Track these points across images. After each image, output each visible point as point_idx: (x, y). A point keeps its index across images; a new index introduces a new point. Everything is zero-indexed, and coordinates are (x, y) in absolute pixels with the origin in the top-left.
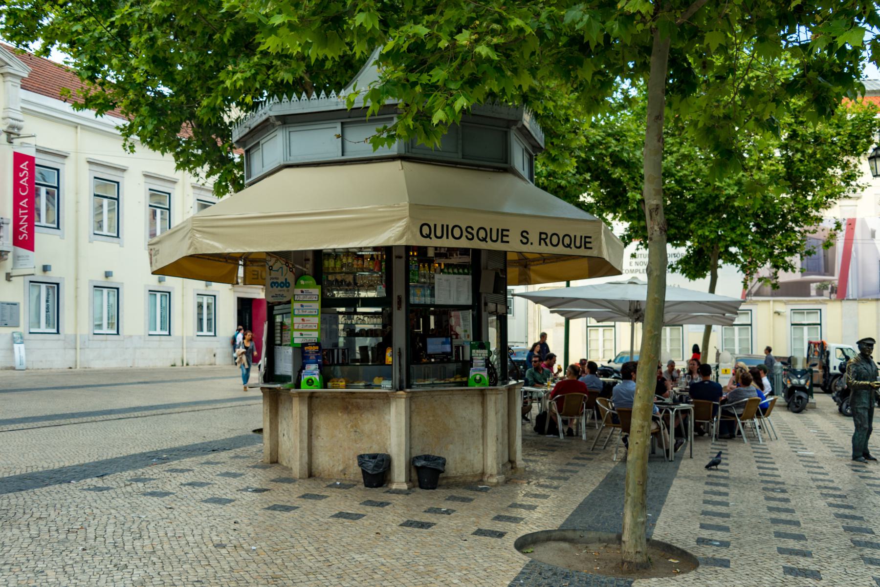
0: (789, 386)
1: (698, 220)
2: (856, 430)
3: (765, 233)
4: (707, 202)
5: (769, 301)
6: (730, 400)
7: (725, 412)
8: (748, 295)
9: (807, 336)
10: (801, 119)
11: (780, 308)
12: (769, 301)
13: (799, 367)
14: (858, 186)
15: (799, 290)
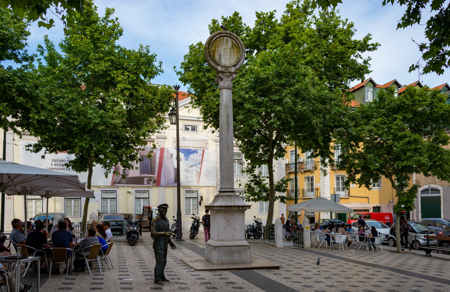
0: (128, 231)
1: (79, 137)
2: (157, 264)
3: (117, 147)
4: (84, 127)
5: (125, 186)
6: (81, 246)
7: (78, 255)
8: (114, 183)
9: (142, 203)
10: (135, 87)
11: (130, 190)
12: (125, 186)
13: (134, 220)
14: (163, 127)
15: (138, 181)
